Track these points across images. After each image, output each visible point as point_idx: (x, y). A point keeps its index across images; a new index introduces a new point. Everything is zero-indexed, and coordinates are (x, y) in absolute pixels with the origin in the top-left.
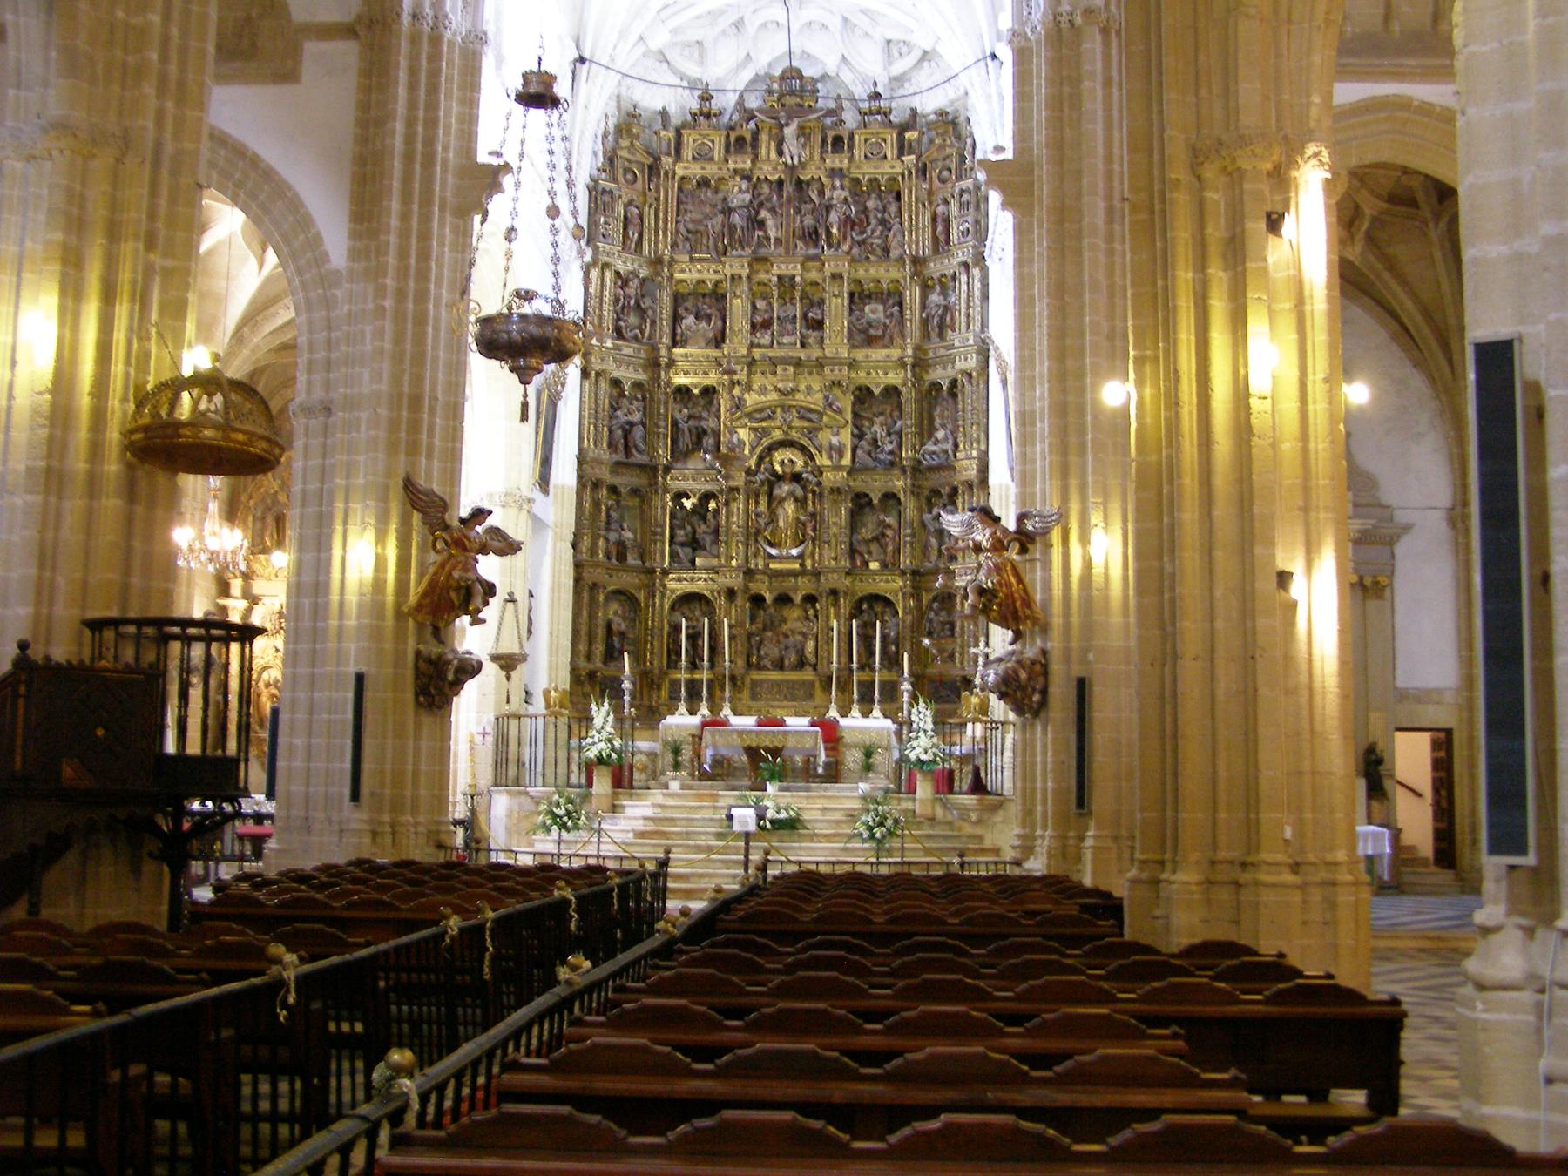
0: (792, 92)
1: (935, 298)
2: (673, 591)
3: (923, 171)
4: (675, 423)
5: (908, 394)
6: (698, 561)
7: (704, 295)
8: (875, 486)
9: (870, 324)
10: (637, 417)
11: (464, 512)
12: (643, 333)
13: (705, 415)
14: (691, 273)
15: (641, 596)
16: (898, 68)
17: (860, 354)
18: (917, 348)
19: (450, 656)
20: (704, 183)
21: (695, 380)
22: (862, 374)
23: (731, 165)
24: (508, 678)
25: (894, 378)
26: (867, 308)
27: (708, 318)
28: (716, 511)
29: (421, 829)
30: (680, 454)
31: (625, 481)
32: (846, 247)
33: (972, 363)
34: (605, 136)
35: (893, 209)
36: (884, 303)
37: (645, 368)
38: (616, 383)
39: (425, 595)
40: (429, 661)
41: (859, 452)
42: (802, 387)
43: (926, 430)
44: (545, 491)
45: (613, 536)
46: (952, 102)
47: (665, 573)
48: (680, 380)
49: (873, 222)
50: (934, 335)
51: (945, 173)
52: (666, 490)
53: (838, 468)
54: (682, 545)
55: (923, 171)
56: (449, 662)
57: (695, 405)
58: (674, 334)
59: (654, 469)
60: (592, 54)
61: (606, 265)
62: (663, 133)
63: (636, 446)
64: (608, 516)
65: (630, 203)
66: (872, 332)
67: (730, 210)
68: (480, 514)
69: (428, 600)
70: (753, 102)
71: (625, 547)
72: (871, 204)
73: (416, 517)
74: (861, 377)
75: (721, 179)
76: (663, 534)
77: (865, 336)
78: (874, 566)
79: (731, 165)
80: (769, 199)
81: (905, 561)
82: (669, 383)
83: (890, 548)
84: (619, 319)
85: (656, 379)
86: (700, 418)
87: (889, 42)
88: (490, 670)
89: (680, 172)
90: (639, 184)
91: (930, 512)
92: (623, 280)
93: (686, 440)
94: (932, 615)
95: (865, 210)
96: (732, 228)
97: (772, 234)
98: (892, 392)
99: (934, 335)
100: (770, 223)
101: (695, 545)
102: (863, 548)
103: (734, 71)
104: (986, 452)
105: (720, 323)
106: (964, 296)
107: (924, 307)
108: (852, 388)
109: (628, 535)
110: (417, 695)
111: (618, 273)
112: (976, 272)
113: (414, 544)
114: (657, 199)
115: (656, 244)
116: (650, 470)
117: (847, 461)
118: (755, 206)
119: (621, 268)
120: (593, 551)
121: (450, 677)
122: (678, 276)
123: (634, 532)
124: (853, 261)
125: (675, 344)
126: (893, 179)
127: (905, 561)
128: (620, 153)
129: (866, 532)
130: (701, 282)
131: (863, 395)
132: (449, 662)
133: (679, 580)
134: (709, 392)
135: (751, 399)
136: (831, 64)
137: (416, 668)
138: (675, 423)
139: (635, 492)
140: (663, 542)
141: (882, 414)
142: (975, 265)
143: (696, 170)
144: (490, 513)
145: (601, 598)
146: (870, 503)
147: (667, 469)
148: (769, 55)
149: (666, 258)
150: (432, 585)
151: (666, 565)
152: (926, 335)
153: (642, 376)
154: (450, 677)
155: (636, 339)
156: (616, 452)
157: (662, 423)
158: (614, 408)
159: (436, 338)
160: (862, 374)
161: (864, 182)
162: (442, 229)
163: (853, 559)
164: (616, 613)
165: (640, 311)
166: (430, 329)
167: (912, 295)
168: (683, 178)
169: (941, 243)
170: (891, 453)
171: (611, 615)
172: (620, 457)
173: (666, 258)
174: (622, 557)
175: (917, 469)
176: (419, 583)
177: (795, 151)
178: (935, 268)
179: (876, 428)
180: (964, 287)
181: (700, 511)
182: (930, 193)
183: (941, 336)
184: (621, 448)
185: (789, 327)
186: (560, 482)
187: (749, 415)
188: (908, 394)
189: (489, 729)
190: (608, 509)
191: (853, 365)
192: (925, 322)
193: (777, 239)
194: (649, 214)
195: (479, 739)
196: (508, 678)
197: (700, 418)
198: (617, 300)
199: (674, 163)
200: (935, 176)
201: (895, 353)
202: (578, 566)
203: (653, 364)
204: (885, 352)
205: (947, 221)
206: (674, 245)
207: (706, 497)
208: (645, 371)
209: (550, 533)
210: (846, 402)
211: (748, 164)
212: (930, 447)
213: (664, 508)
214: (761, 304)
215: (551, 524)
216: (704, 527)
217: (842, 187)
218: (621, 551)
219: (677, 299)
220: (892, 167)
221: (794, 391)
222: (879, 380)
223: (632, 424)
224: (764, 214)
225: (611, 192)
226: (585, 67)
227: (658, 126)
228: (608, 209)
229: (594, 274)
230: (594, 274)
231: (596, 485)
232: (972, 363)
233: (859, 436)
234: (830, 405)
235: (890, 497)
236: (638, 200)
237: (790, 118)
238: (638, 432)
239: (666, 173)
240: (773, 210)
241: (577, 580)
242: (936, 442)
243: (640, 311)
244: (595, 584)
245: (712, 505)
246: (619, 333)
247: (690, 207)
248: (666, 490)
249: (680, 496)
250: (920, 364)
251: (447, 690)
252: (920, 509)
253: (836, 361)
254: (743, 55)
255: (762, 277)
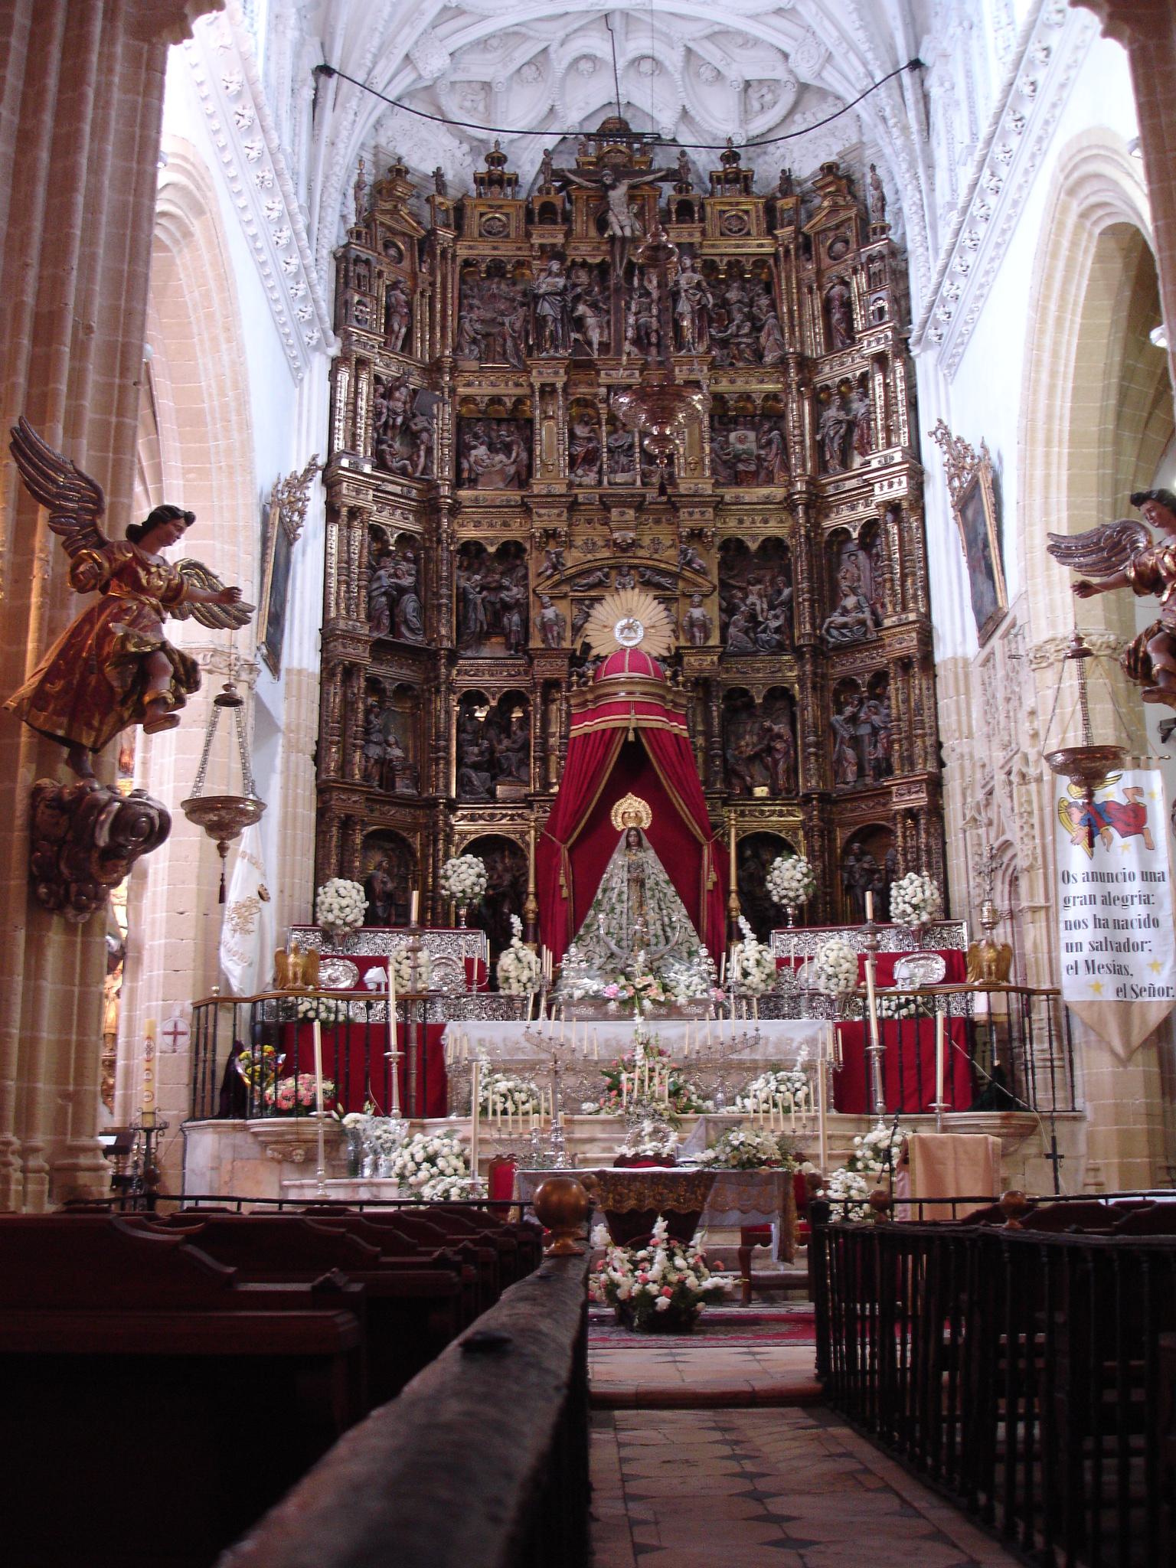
0: (616, 149)
1: (832, 413)
2: (463, 835)
3: (806, 246)
4: (463, 596)
5: (798, 547)
6: (500, 790)
7: (499, 421)
8: (756, 677)
9: (738, 458)
10: (408, 581)
11: (141, 514)
12: (415, 466)
13: (506, 582)
14: (481, 386)
15: (417, 842)
16: (759, 125)
17: (729, 494)
18: (812, 482)
19: (104, 796)
20: (496, 269)
21: (489, 534)
22: (732, 523)
23: (536, 241)
24: (222, 849)
25: (775, 528)
26: (733, 436)
27: (507, 449)
28: (525, 722)
29: (36, 1162)
30: (468, 637)
31: (391, 673)
32: (701, 348)
33: (900, 489)
34: (359, 187)
35: (764, 302)
36: (754, 427)
37: (419, 515)
38: (376, 533)
39: (50, 676)
40: (58, 804)
41: (732, 630)
42: (646, 541)
43: (827, 596)
44: (274, 668)
45: (374, 751)
46: (841, 156)
47: (452, 806)
48: (468, 533)
49: (738, 317)
50: (834, 463)
51: (839, 246)
52: (451, 690)
53: (706, 650)
54: (476, 767)
55: (806, 246)
56: (101, 807)
57: (490, 571)
58: (458, 470)
59: (434, 655)
60: (344, 61)
61: (362, 363)
62: (439, 199)
63: (406, 622)
64: (367, 721)
65: (394, 286)
66: (741, 467)
67: (537, 298)
68: (168, 522)
69: (59, 685)
70: (565, 163)
71: (392, 769)
72: (733, 295)
73: (45, 541)
74: (731, 527)
75: (520, 264)
76: (447, 749)
77: (733, 470)
78: (761, 791)
79: (536, 241)
80: (589, 292)
81: (808, 782)
82: (452, 536)
83: (781, 766)
84: (379, 441)
85: (433, 530)
86: (502, 588)
87: (748, 84)
88: (187, 836)
89: (463, 252)
90: (406, 264)
91: (840, 712)
92: (385, 390)
93: (479, 616)
94: (851, 861)
95: (724, 303)
96: (540, 322)
97: (595, 336)
98: (774, 547)
99: (834, 463)
100: (591, 321)
101: (494, 767)
102: (741, 769)
103: (535, 123)
104: (928, 615)
105: (524, 455)
106: (880, 402)
107: (816, 426)
108: (718, 541)
109: (397, 752)
110: (33, 881)
111: (377, 379)
112: (899, 368)
113: (36, 585)
114: (432, 284)
115: (432, 345)
116: (425, 657)
117: (714, 641)
118: (568, 299)
119: (379, 368)
120: (344, 765)
121: (103, 838)
122: (461, 390)
123: (405, 750)
124: (713, 366)
125: (458, 483)
126: (760, 262)
127: (808, 782)
128: (380, 218)
129: (748, 743)
130: (496, 400)
131: (733, 549)
132: (101, 807)
133: (473, 818)
134: (511, 552)
135: (573, 558)
136: (665, 122)
137: (32, 824)
138: (463, 596)
139: (403, 690)
140: (448, 763)
141: (759, 581)
142: (896, 356)
143: (484, 250)
144: (189, 519)
145: (358, 840)
146: (750, 705)
147: (453, 657)
148: (582, 105)
149: (447, 362)
150: (69, 654)
151: (453, 794)
152: (822, 467)
153: (412, 526)
154: (103, 838)
155: (403, 472)
156: (377, 627)
157: (444, 591)
158: (373, 569)
159: (91, 226)
160: (732, 523)
161: (723, 267)
162: (109, 54)
163: (727, 782)
164: (379, 867)
165: (411, 436)
166: (80, 199)
167: (799, 412)
168: (467, 263)
169: (841, 333)
170: (777, 630)
171: (371, 869)
172: (383, 635)
173: (447, 362)
174: (388, 782)
175: (821, 651)
176: (39, 658)
177: (626, 222)
178: (830, 374)
179: (752, 599)
180: (879, 391)
181: (499, 719)
182: (819, 273)
183: (845, 464)
184: (386, 621)
185: (624, 460)
186: (295, 665)
187: (569, 580)
188: (798, 547)
189: (181, 1027)
190: (368, 711)
191: (719, 506)
192: (819, 447)
193: (600, 344)
194: (421, 313)
195: (163, 1042)
196: (222, 849)
197: (502, 588)
198: (378, 415)
199: (456, 239)
200: (823, 251)
201: (778, 492)
202: (323, 790)
203: (428, 508)
204: (764, 491)
205: (847, 306)
206: (457, 349)
207: (512, 699)
208: (418, 520)
209: (280, 740)
210: (710, 561)
211: (560, 239)
212: (837, 619)
213: (448, 713)
214: (581, 431)
215: (283, 727)
216: (506, 742)
217: (694, 270)
218: (386, 770)
219: (461, 424)
220: (758, 245)
221: (635, 544)
222: (757, 531)
223: (402, 590)
224: (581, 309)
225: (367, 262)
226: (333, 82)
227: (432, 189)
228: (362, 284)
229: (344, 377)
230: (344, 377)
231: (350, 671)
232: (900, 489)
233: (729, 610)
234: (689, 563)
235: (780, 695)
236: (407, 285)
237: (617, 180)
238: (410, 603)
239: (444, 252)
240: (594, 306)
241: (322, 813)
242: (845, 612)
243: (411, 436)
244: (348, 817)
245: (517, 714)
246: (381, 463)
247: (476, 302)
248: (451, 690)
249: (473, 698)
250: (817, 503)
251: (94, 868)
252: (824, 709)
253: (695, 500)
254: (546, 108)
255: (583, 390)
